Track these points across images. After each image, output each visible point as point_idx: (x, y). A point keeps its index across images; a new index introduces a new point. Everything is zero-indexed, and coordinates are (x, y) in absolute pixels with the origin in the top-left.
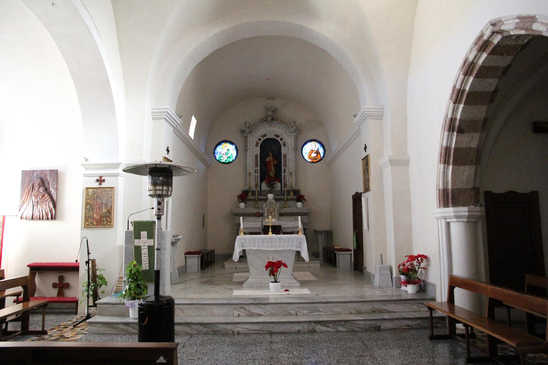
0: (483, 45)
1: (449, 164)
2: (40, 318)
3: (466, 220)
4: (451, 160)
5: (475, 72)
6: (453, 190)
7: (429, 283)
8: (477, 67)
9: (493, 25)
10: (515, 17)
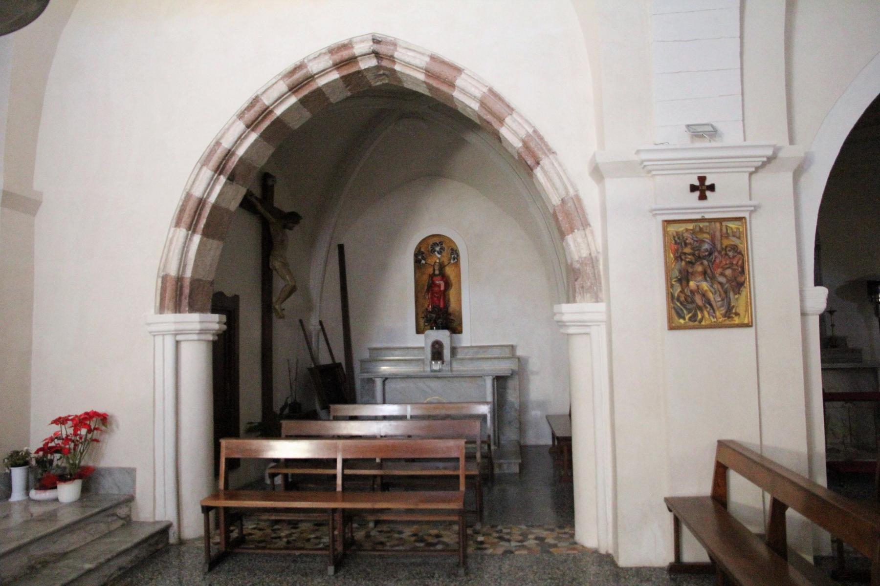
1: (194, 232)
2: (689, 557)
3: (211, 338)
4: (202, 224)
6: (194, 282)
7: (102, 469)
9: (376, 41)
10: (429, 53)
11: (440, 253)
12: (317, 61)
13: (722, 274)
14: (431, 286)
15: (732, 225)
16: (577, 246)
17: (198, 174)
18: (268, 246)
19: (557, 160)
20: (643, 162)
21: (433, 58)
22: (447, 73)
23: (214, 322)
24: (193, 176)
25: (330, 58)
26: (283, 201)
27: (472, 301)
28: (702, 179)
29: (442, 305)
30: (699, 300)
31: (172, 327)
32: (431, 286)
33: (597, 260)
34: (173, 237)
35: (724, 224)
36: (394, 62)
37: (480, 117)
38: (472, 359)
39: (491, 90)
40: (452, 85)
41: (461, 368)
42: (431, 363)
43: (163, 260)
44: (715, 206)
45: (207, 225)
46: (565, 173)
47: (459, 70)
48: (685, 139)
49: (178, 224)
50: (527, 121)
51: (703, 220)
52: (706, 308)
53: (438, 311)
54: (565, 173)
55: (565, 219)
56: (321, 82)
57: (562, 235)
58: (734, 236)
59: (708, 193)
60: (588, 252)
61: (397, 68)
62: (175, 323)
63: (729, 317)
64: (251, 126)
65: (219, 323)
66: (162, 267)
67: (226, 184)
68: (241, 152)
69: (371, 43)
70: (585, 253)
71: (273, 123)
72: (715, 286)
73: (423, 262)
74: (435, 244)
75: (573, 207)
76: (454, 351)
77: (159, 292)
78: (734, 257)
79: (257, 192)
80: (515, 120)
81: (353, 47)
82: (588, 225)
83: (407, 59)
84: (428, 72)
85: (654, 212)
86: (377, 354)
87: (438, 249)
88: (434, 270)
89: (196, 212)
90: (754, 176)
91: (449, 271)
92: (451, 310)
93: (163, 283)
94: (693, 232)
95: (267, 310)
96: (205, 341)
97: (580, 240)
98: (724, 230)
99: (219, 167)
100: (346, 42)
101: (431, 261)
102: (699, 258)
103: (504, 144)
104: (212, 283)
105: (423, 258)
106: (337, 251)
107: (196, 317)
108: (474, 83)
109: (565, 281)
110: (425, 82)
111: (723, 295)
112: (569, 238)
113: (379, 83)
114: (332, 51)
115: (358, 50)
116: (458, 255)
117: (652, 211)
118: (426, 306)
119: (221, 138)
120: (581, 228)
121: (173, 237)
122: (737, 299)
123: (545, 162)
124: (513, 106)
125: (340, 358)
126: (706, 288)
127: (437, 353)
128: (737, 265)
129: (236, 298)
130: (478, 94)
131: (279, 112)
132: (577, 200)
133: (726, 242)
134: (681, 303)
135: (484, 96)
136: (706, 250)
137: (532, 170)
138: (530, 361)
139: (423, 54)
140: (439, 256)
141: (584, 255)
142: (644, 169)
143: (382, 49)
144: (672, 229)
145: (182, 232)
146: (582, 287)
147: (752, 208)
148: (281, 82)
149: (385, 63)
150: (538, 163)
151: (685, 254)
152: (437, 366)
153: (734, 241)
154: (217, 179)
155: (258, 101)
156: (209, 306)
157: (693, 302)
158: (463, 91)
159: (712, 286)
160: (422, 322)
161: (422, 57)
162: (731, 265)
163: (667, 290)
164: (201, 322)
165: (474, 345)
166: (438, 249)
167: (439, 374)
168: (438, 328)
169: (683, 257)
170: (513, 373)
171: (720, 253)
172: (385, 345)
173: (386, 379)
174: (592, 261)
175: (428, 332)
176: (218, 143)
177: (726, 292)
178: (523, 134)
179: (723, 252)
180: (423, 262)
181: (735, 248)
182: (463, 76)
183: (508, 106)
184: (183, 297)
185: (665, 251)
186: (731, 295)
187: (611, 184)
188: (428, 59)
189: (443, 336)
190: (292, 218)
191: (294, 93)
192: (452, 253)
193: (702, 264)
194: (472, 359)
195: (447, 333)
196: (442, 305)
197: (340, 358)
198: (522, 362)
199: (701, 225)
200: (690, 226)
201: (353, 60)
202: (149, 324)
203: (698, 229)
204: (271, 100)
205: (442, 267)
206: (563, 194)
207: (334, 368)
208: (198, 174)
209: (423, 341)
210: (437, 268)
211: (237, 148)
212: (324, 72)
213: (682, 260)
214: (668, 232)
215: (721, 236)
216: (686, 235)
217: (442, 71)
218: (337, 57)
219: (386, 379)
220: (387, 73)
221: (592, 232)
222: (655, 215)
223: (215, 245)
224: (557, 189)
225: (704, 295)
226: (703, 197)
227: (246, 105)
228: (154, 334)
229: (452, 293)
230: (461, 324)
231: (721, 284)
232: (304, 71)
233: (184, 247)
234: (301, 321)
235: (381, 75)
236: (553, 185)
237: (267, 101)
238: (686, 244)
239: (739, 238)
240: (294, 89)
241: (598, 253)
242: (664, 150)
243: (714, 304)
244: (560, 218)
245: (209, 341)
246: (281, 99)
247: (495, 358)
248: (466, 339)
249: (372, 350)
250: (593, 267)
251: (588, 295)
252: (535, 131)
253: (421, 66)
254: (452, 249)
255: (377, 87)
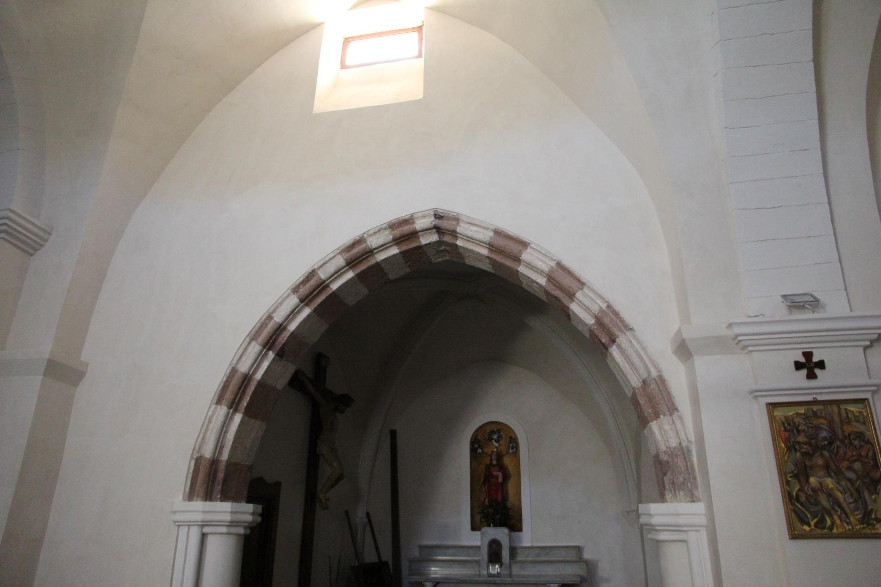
0: (404, 233)
1: (236, 410)
3: (241, 531)
4: (245, 404)
5: (363, 267)
6: (230, 464)
8: (371, 262)
9: (438, 216)
11: (497, 441)
12: (377, 236)
13: (849, 468)
14: (489, 477)
15: (852, 408)
16: (663, 434)
17: (246, 349)
18: (317, 429)
19: (635, 337)
20: (737, 336)
21: (497, 232)
22: (513, 247)
23: (247, 512)
24: (241, 351)
25: (390, 233)
26: (335, 383)
27: (533, 495)
28: (808, 355)
29: (500, 499)
30: (824, 502)
31: (199, 517)
32: (489, 477)
33: (689, 451)
34: (213, 415)
35: (842, 407)
36: (456, 237)
37: (547, 293)
38: (534, 562)
39: (559, 264)
40: (517, 260)
41: (523, 573)
42: (488, 567)
43: (200, 440)
44: (832, 383)
45: (250, 404)
46: (646, 352)
47: (524, 244)
48: (781, 311)
49: (219, 401)
50: (599, 296)
51: (815, 402)
52: (836, 511)
53: (496, 506)
54: (646, 352)
55: (644, 405)
56: (381, 257)
57: (644, 422)
58: (857, 421)
59: (817, 371)
60: (677, 441)
61: (459, 243)
62: (204, 512)
63: (868, 524)
64: (305, 300)
65: (253, 514)
66: (197, 448)
67: (274, 359)
68: (293, 327)
69: (433, 219)
70: (674, 443)
71: (327, 299)
72: (843, 483)
73: (480, 451)
74: (493, 432)
75: (656, 388)
76: (513, 551)
77: (190, 475)
78: (861, 447)
79: (309, 371)
80: (586, 296)
81: (414, 223)
82: (676, 409)
83: (470, 234)
84: (491, 247)
85: (755, 394)
86: (428, 554)
87: (495, 437)
88: (491, 460)
89: (239, 389)
90: (869, 351)
91: (507, 461)
92: (509, 505)
93: (196, 465)
94: (806, 417)
95: (311, 499)
96: (235, 534)
97: (667, 427)
98: (843, 414)
99: (268, 341)
100: (407, 217)
101: (488, 450)
102: (817, 449)
103: (574, 322)
104: (250, 468)
105: (480, 446)
106: (389, 437)
107: (227, 506)
108: (541, 257)
109: (635, 473)
110: (488, 257)
111: (855, 494)
112: (654, 425)
113: (439, 260)
114: (392, 226)
115: (420, 224)
116: (517, 444)
117: (752, 392)
118: (482, 499)
119: (274, 311)
120: (667, 413)
121: (213, 415)
122: (875, 501)
123: (622, 339)
124: (584, 280)
125: (387, 555)
126: (831, 486)
127: (495, 555)
128: (867, 456)
129: (278, 484)
130: (546, 269)
131: (334, 286)
132: (661, 381)
133: (848, 429)
134: (802, 505)
135: (552, 270)
136: (825, 439)
137: (607, 349)
138: (600, 565)
139: (487, 229)
140: (497, 444)
141: (674, 445)
142: (738, 344)
143: (444, 224)
144: (779, 413)
145: (223, 410)
146: (673, 483)
147: (875, 388)
148: (339, 257)
149: (447, 239)
150: (614, 341)
151: (799, 443)
152: (495, 569)
153: (859, 427)
154: (266, 354)
155: (314, 276)
156: (245, 494)
157: (817, 503)
158: (530, 266)
159: (839, 483)
160: (478, 517)
161: (486, 232)
162: (859, 458)
163: (782, 487)
164: (232, 513)
165: (535, 545)
166: (495, 437)
167: (497, 580)
168: (495, 525)
169: (797, 447)
170: (583, 580)
171: (842, 441)
172: (439, 543)
173: (438, 583)
174: (683, 452)
175: (485, 529)
176: (270, 317)
177: (858, 490)
178: (595, 309)
179: (847, 441)
180: (480, 451)
181: (860, 436)
182: (529, 250)
183: (579, 280)
184: (216, 484)
185: (774, 440)
186: (866, 494)
187: (701, 363)
188: (491, 234)
189: (501, 534)
190: (344, 401)
191: (351, 268)
192: (510, 442)
193: (822, 455)
194: (534, 562)
195: (505, 530)
196: (500, 499)
197: (387, 555)
198: (591, 567)
199: (815, 408)
200: (802, 410)
201: (414, 234)
202: (174, 512)
203: (810, 413)
204: (328, 275)
205: (500, 457)
206: (645, 375)
207: (381, 565)
208: (246, 349)
209: (476, 539)
210: (494, 457)
211: (289, 323)
212: (383, 247)
213: (796, 451)
214: (775, 417)
215: (841, 421)
216: (797, 420)
217: (507, 247)
218: (398, 232)
219: (438, 583)
220: (448, 248)
221: (681, 419)
222: (756, 397)
223: (258, 426)
224: (636, 370)
225: (830, 495)
226: (811, 376)
227: (302, 279)
228: (179, 525)
229: (511, 486)
230: (520, 520)
231: (850, 480)
232: (363, 246)
233: (223, 427)
234: (346, 512)
235: (442, 251)
236: (632, 364)
237: (322, 275)
238: (799, 431)
239: (864, 423)
240: (351, 264)
241: (689, 442)
242: (762, 323)
243: (845, 505)
244: (642, 402)
245: (239, 535)
246: (338, 273)
247: (561, 562)
248: (527, 538)
249: (422, 547)
250: (685, 459)
251: (682, 493)
252: (609, 306)
253: (485, 240)
254: (511, 438)
255: (438, 263)
